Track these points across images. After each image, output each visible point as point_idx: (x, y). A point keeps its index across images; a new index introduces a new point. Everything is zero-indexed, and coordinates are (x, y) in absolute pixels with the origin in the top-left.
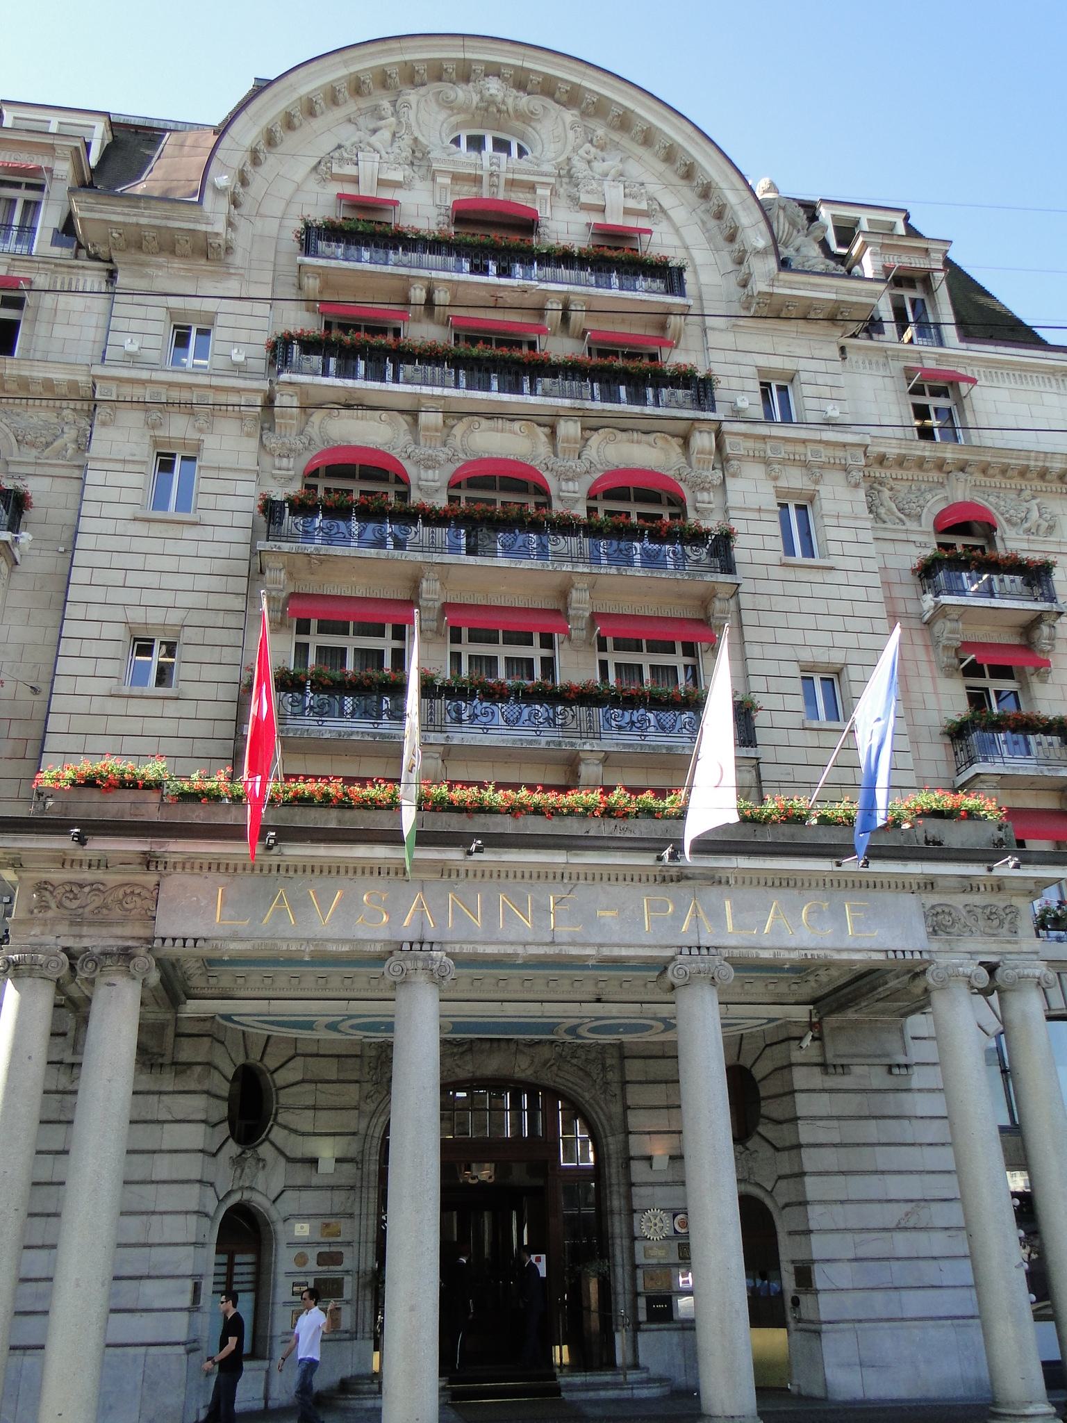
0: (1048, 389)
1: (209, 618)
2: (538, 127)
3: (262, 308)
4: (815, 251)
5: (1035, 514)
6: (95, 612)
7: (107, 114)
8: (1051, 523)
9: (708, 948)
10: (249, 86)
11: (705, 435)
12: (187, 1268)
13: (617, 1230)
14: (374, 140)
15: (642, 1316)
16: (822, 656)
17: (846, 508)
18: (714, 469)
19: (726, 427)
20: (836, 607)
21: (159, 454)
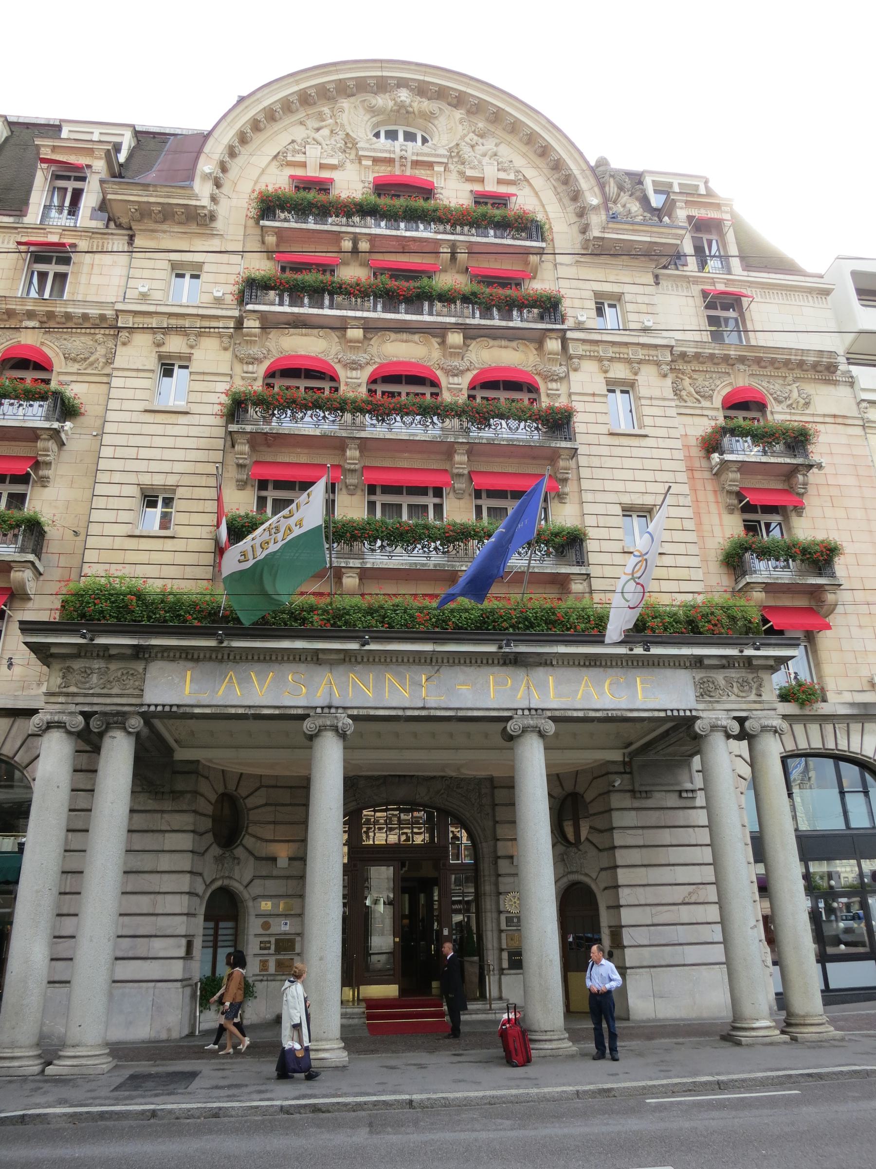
0: (806, 304)
1: (196, 480)
2: (436, 122)
3: (236, 258)
4: (635, 207)
5: (795, 394)
6: (117, 477)
7: (133, 127)
8: (807, 400)
9: (536, 710)
11: (554, 341)
12: (182, 931)
13: (488, 907)
14: (317, 136)
15: (505, 965)
16: (158, 480)
17: (657, 393)
18: (561, 365)
19: (569, 334)
20: (648, 464)
21: (163, 364)
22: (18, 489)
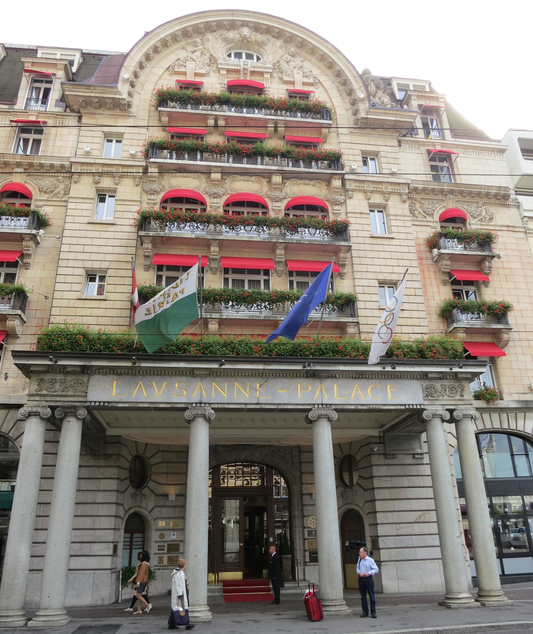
0: (491, 158)
2: (265, 48)
3: (144, 130)
4: (386, 99)
5: (484, 213)
6: (71, 263)
7: (81, 50)
8: (491, 217)
10: (142, 35)
11: (337, 181)
12: (111, 539)
13: (297, 525)
14: (193, 56)
15: (307, 559)
17: (400, 212)
18: (341, 195)
19: (346, 177)
20: (395, 255)
21: (99, 195)
22: (11, 270)
